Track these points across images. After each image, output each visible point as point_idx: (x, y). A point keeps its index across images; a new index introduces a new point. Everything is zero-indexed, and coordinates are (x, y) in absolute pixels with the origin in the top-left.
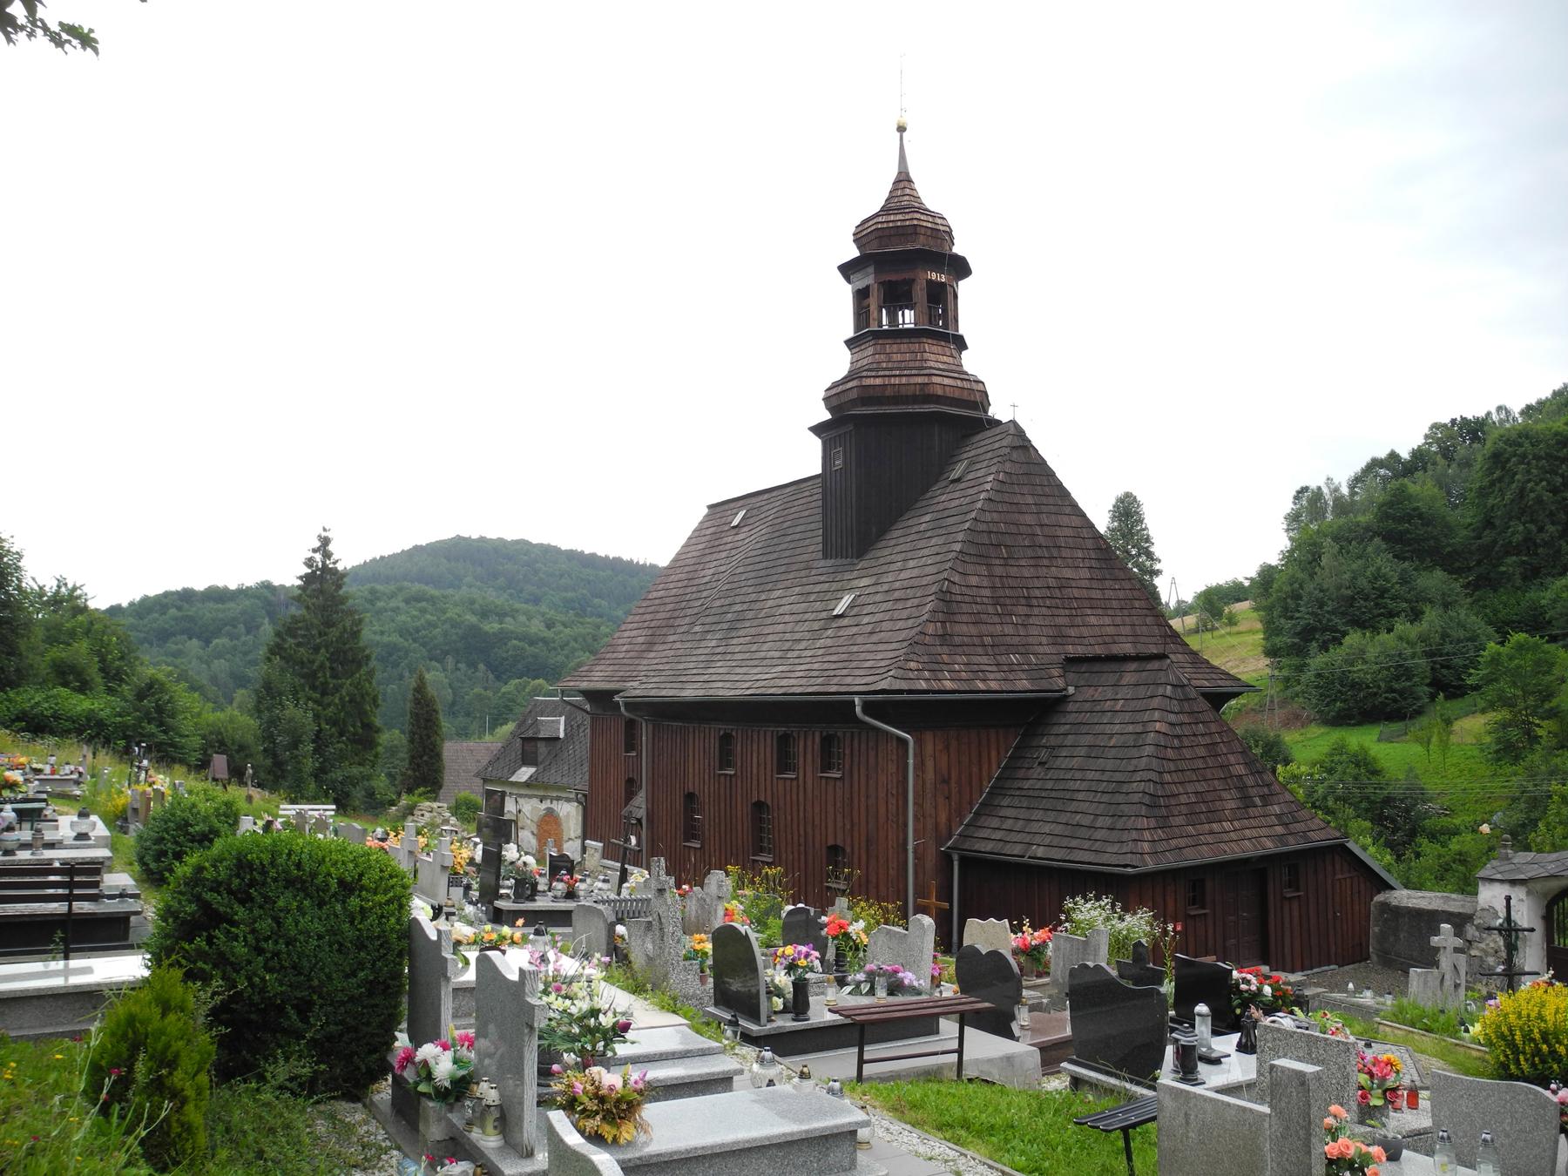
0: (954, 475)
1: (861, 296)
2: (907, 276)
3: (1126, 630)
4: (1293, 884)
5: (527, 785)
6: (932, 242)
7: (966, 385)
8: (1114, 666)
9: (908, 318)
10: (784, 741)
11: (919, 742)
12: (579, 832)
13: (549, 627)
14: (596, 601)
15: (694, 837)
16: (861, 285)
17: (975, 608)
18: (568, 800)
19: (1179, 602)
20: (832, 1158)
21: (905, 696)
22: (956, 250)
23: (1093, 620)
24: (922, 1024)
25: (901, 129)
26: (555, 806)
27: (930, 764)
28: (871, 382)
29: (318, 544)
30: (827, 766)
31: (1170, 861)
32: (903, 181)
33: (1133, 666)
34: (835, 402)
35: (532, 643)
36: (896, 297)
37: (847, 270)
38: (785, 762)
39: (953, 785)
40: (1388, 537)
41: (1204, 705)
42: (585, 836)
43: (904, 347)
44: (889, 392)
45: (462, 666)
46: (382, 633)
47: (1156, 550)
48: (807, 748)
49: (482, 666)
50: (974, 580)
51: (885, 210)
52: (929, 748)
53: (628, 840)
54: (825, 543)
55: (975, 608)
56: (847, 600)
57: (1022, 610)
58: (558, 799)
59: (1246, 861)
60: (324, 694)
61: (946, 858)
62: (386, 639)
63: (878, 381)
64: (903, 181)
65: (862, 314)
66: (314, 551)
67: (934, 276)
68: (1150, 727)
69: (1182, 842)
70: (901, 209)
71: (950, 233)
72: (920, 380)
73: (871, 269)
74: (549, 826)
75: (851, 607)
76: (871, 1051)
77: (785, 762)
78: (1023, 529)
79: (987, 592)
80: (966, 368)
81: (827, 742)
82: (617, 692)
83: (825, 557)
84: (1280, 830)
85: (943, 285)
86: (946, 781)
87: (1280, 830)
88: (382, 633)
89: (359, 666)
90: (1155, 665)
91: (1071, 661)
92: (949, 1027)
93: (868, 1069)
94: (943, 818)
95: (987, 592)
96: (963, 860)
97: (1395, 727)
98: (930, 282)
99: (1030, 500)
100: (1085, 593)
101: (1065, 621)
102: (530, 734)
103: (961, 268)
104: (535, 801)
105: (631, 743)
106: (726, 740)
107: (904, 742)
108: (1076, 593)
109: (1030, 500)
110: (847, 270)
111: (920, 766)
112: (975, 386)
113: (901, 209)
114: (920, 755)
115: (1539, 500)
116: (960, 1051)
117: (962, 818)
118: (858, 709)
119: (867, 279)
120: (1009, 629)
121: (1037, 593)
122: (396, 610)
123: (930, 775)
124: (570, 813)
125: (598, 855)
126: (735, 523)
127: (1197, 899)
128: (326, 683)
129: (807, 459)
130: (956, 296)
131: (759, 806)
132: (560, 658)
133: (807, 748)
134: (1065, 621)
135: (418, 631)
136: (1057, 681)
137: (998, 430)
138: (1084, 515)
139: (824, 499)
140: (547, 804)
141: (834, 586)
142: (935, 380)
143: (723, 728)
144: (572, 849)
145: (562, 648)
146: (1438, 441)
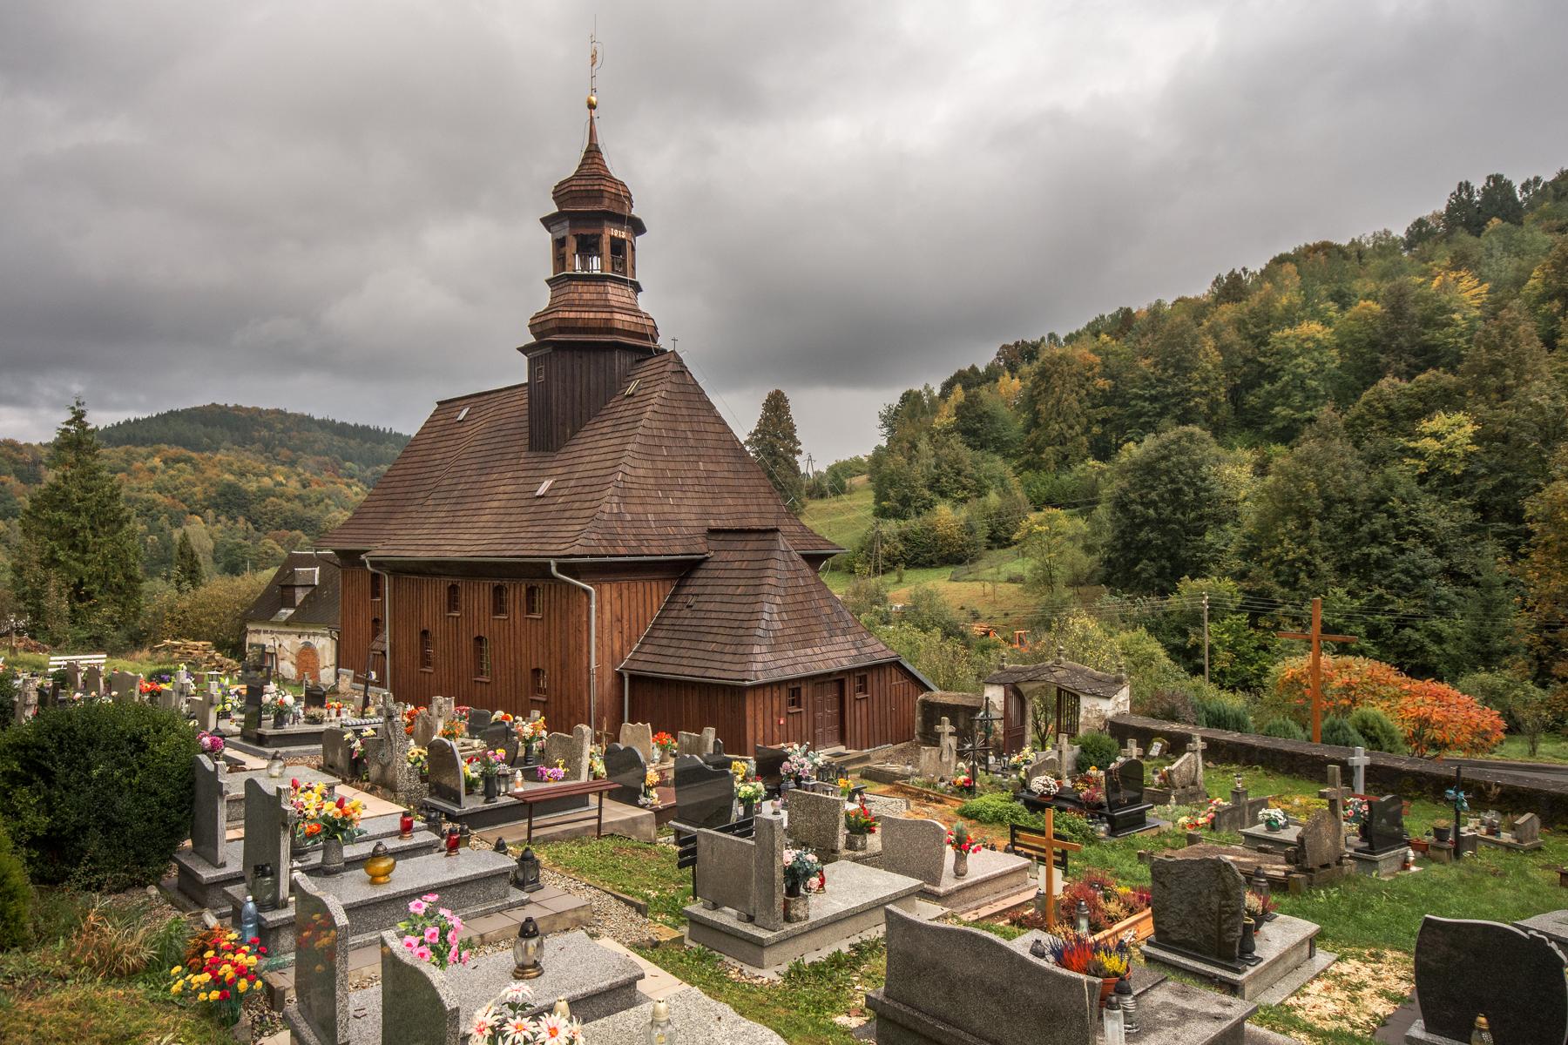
0: (630, 391)
1: (560, 244)
2: (597, 231)
3: (755, 508)
4: (863, 689)
5: (287, 623)
6: (615, 204)
7: (640, 321)
8: (742, 537)
9: (596, 265)
10: (498, 591)
11: (600, 592)
12: (333, 661)
13: (304, 487)
14: (348, 464)
15: (429, 664)
16: (559, 235)
17: (642, 493)
18: (323, 635)
19: (816, 473)
20: (493, 891)
21: (588, 559)
22: (634, 212)
23: (730, 501)
24: (575, 800)
25: (592, 106)
26: (311, 640)
27: (607, 607)
28: (566, 315)
29: (71, 417)
30: (531, 610)
31: (776, 675)
32: (593, 152)
33: (754, 537)
34: (538, 329)
35: (289, 500)
36: (588, 247)
37: (548, 222)
38: (499, 607)
39: (625, 622)
40: (965, 432)
41: (803, 564)
42: (338, 665)
43: (592, 289)
44: (580, 324)
45: (223, 518)
46: (140, 490)
47: (798, 436)
48: (516, 594)
49: (241, 519)
50: (641, 472)
51: (578, 175)
52: (607, 595)
53: (369, 675)
54: (531, 438)
55: (642, 493)
56: (547, 484)
57: (679, 494)
58: (315, 634)
59: (830, 674)
60: (85, 551)
61: (620, 675)
62: (145, 496)
63: (572, 315)
64: (593, 152)
65: (560, 259)
66: (69, 423)
67: (616, 233)
68: (765, 581)
69: (784, 663)
70: (591, 176)
71: (629, 199)
72: (604, 316)
73: (567, 223)
74: (307, 657)
75: (550, 490)
76: (537, 821)
77: (499, 607)
78: (679, 434)
79: (652, 481)
80: (640, 308)
81: (531, 591)
82: (365, 552)
83: (530, 450)
84: (854, 652)
85: (623, 241)
86: (620, 620)
87: (854, 652)
88: (140, 490)
89: (121, 526)
90: (770, 536)
91: (713, 532)
92: (593, 800)
93: (535, 834)
94: (617, 647)
95: (652, 481)
96: (631, 677)
97: (961, 569)
98: (612, 238)
99: (684, 412)
100: (724, 482)
101: (709, 502)
102: (288, 582)
103: (638, 227)
104: (294, 637)
105: (376, 591)
106: (453, 589)
107: (587, 592)
108: (718, 482)
109: (684, 412)
110: (548, 222)
111: (600, 610)
112: (646, 322)
113: (591, 176)
114: (600, 602)
115: (1069, 406)
116: (599, 817)
117: (630, 645)
118: (554, 569)
119: (564, 230)
120: (666, 508)
121: (689, 481)
122: (153, 470)
123: (607, 615)
124: (325, 646)
125: (349, 680)
126: (461, 417)
127: (796, 702)
128: (85, 542)
129: (517, 372)
130: (633, 249)
131: (479, 639)
132: (315, 513)
133: (516, 594)
134: (709, 502)
135: (176, 489)
136: (700, 547)
137: (665, 357)
138: (724, 424)
139: (530, 404)
140: (305, 639)
141: (537, 473)
142: (617, 316)
143: (450, 581)
144: (326, 676)
145: (317, 504)
146: (1006, 359)
